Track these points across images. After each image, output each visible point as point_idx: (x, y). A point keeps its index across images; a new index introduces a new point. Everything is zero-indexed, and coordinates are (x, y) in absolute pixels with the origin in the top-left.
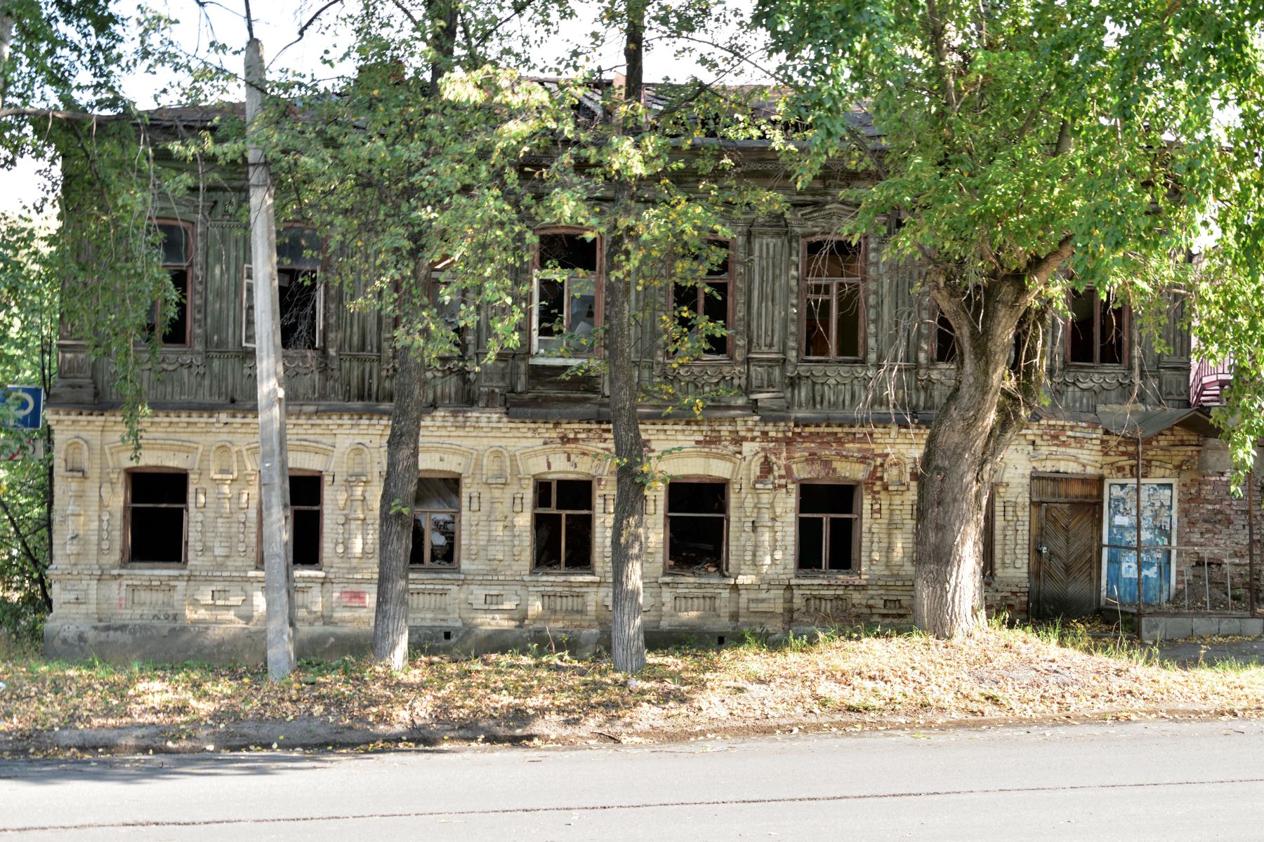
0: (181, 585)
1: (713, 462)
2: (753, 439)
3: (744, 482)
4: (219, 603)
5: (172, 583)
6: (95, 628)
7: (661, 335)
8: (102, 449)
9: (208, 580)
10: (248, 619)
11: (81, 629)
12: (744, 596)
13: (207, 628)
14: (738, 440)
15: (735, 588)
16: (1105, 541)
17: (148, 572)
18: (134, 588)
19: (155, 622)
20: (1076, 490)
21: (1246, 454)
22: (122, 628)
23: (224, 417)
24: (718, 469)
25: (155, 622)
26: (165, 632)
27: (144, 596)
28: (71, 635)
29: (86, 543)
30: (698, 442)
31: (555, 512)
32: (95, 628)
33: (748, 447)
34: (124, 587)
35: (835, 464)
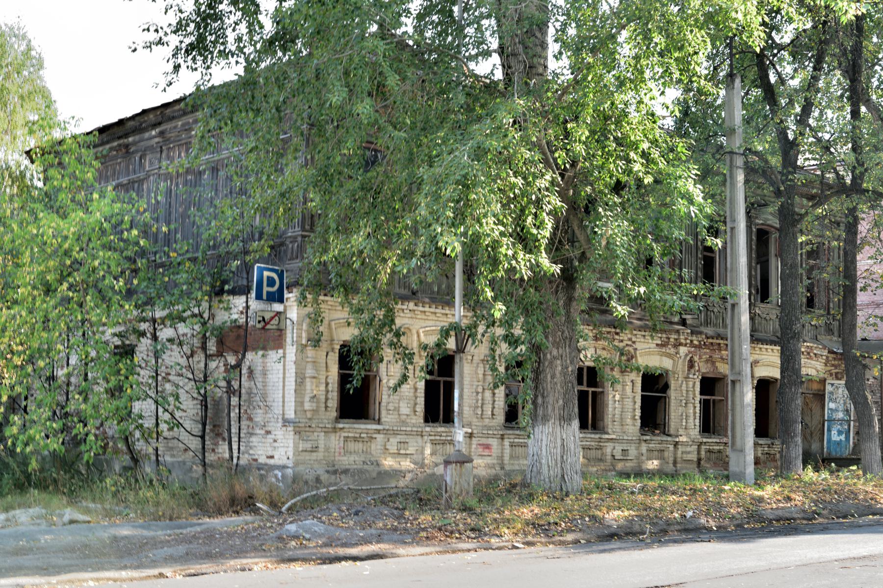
0: (380, 437)
1: (664, 358)
2: (686, 345)
3: (680, 373)
4: (402, 452)
5: (374, 436)
6: (328, 472)
7: (282, 140)
8: (711, 420)
9: (395, 433)
10: (423, 466)
11: (318, 472)
12: (681, 448)
13: (224, 439)
14: (678, 344)
15: (676, 444)
16: (826, 418)
17: (363, 426)
18: (346, 439)
19: (366, 467)
20: (815, 386)
21: (876, 372)
22: (346, 472)
23: (411, 305)
24: (667, 364)
25: (366, 467)
26: (374, 475)
27: (352, 446)
28: (311, 478)
29: (318, 402)
30: (657, 345)
31: (586, 389)
32: (328, 472)
33: (683, 350)
34: (342, 439)
35: (718, 364)
